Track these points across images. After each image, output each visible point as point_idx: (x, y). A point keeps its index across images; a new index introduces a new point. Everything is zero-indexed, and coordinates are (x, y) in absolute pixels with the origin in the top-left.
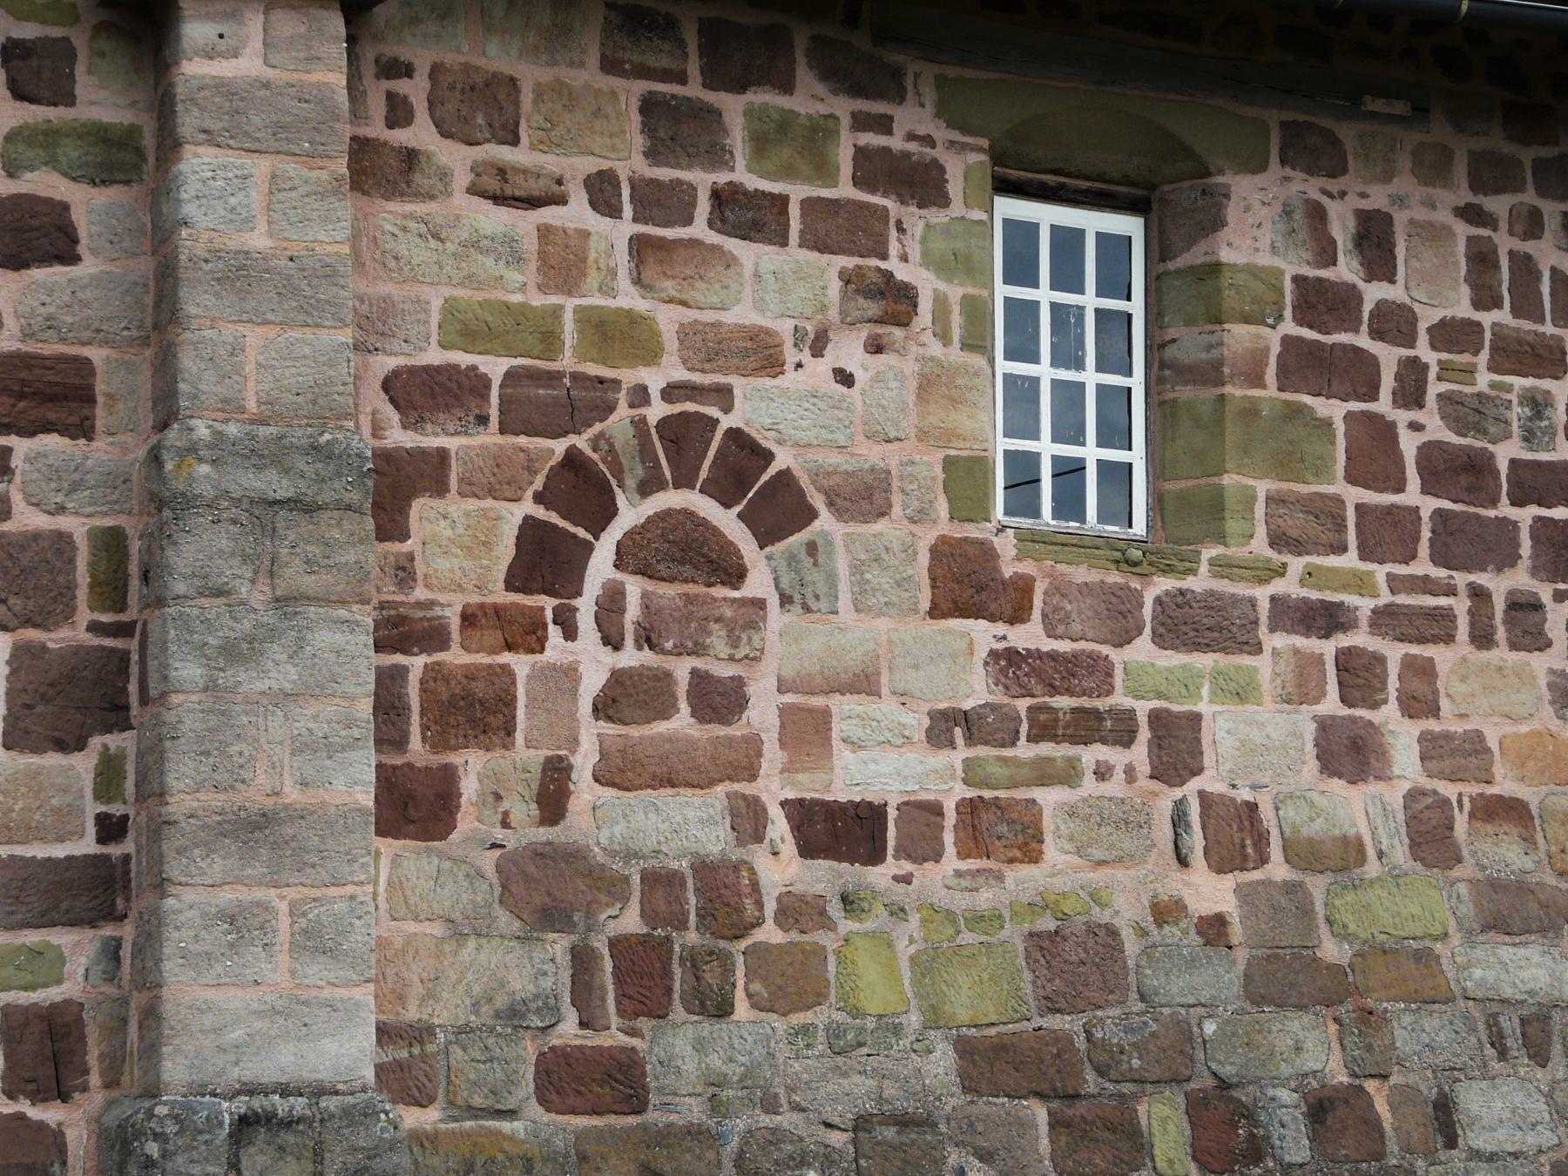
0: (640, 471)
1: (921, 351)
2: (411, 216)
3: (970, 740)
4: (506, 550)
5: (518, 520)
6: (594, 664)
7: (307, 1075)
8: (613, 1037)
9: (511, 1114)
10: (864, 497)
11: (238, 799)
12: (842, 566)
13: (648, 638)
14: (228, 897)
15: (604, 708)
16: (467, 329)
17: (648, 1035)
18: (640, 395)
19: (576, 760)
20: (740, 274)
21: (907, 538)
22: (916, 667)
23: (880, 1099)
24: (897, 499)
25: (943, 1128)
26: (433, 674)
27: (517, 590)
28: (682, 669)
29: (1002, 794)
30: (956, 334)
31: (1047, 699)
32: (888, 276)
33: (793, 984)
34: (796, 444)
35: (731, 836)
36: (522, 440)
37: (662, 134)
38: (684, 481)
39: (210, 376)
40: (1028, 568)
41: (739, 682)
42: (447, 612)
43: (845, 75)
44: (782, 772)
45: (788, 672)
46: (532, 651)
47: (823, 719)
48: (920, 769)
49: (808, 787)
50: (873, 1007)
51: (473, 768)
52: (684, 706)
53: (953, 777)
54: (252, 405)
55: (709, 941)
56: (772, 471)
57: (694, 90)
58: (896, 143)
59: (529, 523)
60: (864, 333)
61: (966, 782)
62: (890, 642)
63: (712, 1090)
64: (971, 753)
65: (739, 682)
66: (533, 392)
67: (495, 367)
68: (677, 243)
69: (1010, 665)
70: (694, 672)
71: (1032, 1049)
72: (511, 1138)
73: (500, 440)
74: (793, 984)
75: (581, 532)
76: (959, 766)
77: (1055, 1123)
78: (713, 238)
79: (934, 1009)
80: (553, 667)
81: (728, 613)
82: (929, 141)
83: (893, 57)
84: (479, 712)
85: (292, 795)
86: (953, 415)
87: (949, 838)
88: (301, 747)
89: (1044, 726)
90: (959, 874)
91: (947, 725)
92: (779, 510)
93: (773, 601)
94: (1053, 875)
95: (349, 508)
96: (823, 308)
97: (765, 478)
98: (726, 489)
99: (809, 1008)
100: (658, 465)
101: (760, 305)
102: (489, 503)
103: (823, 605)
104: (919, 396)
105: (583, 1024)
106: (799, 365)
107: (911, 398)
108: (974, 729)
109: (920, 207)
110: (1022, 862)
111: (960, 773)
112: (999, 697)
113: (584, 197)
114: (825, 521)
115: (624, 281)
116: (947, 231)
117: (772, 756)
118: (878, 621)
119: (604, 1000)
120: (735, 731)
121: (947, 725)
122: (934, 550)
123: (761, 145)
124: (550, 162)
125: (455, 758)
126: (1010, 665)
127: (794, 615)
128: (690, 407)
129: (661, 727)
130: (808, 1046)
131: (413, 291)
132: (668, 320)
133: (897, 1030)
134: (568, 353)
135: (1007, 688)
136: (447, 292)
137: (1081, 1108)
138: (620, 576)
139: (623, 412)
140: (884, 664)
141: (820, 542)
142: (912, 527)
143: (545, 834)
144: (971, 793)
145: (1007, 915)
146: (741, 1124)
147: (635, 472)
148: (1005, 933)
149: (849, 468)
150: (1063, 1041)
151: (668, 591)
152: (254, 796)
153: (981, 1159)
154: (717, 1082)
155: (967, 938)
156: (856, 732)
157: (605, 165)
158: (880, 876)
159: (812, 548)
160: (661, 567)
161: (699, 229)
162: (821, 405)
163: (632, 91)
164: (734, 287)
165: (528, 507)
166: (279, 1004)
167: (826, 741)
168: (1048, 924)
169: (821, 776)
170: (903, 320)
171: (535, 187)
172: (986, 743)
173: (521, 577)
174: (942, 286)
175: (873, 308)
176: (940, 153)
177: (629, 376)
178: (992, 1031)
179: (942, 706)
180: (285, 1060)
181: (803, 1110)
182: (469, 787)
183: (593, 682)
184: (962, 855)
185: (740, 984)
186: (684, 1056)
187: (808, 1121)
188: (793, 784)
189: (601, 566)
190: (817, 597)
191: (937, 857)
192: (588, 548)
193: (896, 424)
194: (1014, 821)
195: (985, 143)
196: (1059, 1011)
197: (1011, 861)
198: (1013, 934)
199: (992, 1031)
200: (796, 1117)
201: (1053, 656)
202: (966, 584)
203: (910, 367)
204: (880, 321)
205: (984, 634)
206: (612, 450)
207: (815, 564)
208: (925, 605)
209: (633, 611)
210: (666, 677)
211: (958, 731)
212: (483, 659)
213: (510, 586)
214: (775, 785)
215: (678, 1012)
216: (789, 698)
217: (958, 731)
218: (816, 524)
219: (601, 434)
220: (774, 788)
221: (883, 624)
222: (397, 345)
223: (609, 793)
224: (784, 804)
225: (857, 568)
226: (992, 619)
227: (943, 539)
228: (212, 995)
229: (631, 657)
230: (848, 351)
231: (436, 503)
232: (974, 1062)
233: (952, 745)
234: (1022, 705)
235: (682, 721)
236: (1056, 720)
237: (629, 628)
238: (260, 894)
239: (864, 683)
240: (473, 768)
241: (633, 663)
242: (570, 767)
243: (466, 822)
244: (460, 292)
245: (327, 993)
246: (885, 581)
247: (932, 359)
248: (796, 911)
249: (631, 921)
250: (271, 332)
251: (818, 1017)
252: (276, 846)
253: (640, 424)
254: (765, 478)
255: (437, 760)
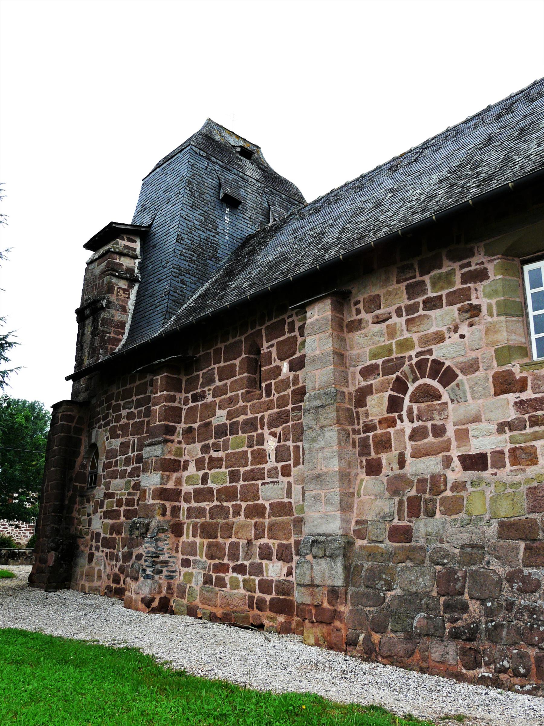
0: (412, 377)
1: (485, 321)
2: (361, 334)
3: (511, 430)
4: (386, 404)
5: (388, 396)
6: (407, 427)
7: (328, 532)
8: (405, 523)
9: (381, 542)
10: (471, 367)
11: (315, 472)
12: (467, 388)
13: (419, 418)
14: (314, 493)
15: (411, 438)
16: (374, 356)
17: (414, 522)
18: (410, 358)
19: (406, 452)
20: (432, 319)
21: (485, 376)
22: (492, 411)
23: (471, 540)
24: (481, 365)
25: (486, 549)
26: (375, 436)
27: (389, 413)
28: (429, 424)
29: (522, 445)
30: (495, 313)
31: (534, 413)
32: (471, 305)
33: (453, 507)
34: (450, 358)
35: (442, 467)
36: (387, 377)
37: (411, 292)
38: (423, 376)
39: (310, 383)
40: (524, 374)
41: (444, 425)
42: (376, 421)
43: (454, 258)
44: (457, 447)
45: (455, 420)
46: (393, 427)
47: (467, 431)
48: (496, 441)
49: (464, 451)
50: (476, 513)
51: (384, 457)
52: (431, 434)
53: (506, 442)
54: (317, 387)
55: (431, 496)
56: (445, 367)
57: (418, 278)
58: (473, 268)
59: (390, 396)
60: (467, 322)
61: (511, 443)
62: (483, 406)
63: (428, 536)
64: (511, 434)
65: (444, 425)
66: (387, 365)
67: (380, 362)
68: (417, 317)
69: (521, 405)
70: (432, 425)
71: (523, 525)
72: (381, 548)
73: (382, 378)
74: (453, 507)
75: (401, 396)
76: (508, 439)
77: (527, 548)
78: (425, 313)
79: (495, 513)
80: (398, 430)
81: (438, 407)
82: (482, 263)
83: (469, 246)
84: (384, 444)
85: (324, 470)
86: (496, 336)
87: (507, 460)
88: (325, 459)
89: (534, 422)
90: (511, 471)
91: (502, 427)
92: (448, 377)
93: (449, 401)
94: (542, 469)
95: (331, 404)
96: (454, 320)
97: (443, 369)
98: (433, 376)
99: (457, 514)
100: (416, 374)
101: (437, 326)
102: (382, 393)
103: (462, 400)
104: (486, 334)
105: (399, 520)
106: (450, 337)
107: (484, 335)
108: (512, 427)
109: (481, 282)
110: (531, 465)
111: (508, 440)
112: (519, 415)
113: (395, 314)
114: (461, 377)
115: (405, 332)
116: (490, 285)
117: (454, 443)
118: (479, 401)
119: (404, 513)
120: (444, 438)
121: (502, 427)
122: (493, 377)
123: (434, 285)
124: (387, 310)
125: (380, 455)
126: (521, 405)
127: (455, 404)
128: (422, 357)
129: (425, 441)
130: (455, 525)
131: (362, 350)
132: (415, 337)
133: (481, 519)
134: (394, 353)
135: (520, 412)
136: (369, 348)
137: (537, 544)
138: (411, 404)
139: (407, 363)
140: (482, 412)
141: (459, 383)
142: (486, 372)
143: (400, 472)
144: (513, 446)
145: (522, 483)
146: (433, 546)
147: (411, 377)
148: (521, 489)
149: (466, 360)
150: (534, 522)
151: (423, 405)
152: (318, 471)
153: (497, 559)
154: (428, 534)
155: (509, 490)
156: (476, 434)
157: (398, 305)
158: (486, 474)
159: (458, 385)
160: (420, 399)
161: (421, 312)
162: (456, 346)
163: (403, 286)
164: (430, 323)
165: (390, 392)
166: (323, 516)
167: (468, 437)
168: (535, 484)
169: (468, 448)
170: (476, 315)
171: (384, 317)
172: (516, 430)
173: (389, 410)
174: (489, 301)
175: (467, 315)
176: (486, 265)
177: (407, 354)
178: (512, 519)
179: (501, 422)
180: (324, 529)
181: (449, 543)
182: (384, 462)
183: (408, 432)
184: (512, 465)
185: (438, 508)
186: (422, 526)
187: (450, 546)
188: (460, 451)
189: (407, 403)
190: (461, 398)
191: (504, 467)
192: (403, 399)
193: (478, 344)
194: (527, 453)
195: (499, 256)
196: (534, 512)
197: (528, 465)
198: (524, 488)
199: (512, 519)
200: (447, 544)
201: (535, 399)
202: (505, 384)
203: (482, 327)
204: (470, 318)
205: (512, 397)
206: (405, 374)
207: (459, 389)
208: (493, 393)
209: (415, 412)
210: (426, 427)
211: (506, 428)
212: (384, 431)
213: (388, 413)
214: (455, 452)
215: (422, 516)
216: (457, 427)
217: (506, 428)
218: (458, 378)
219: (403, 371)
220: (455, 453)
221: (480, 401)
222: (361, 363)
223: (414, 459)
224: (458, 456)
225: (471, 387)
226: (514, 392)
227: (496, 373)
228: (312, 514)
229: (416, 424)
230: (464, 329)
231: (371, 397)
232: (503, 529)
233: (505, 432)
234: (526, 416)
235: (431, 438)
236: (538, 419)
237: (415, 416)
238: (319, 492)
239: (477, 419)
240: (384, 457)
241: (417, 425)
242: (405, 454)
243: (384, 471)
244: (372, 347)
245: (331, 513)
246: (480, 389)
247: (488, 322)
248: (458, 486)
249: (413, 493)
250: (319, 370)
251: (459, 516)
252: (321, 481)
253: (411, 366)
254: (443, 369)
255: (377, 457)
